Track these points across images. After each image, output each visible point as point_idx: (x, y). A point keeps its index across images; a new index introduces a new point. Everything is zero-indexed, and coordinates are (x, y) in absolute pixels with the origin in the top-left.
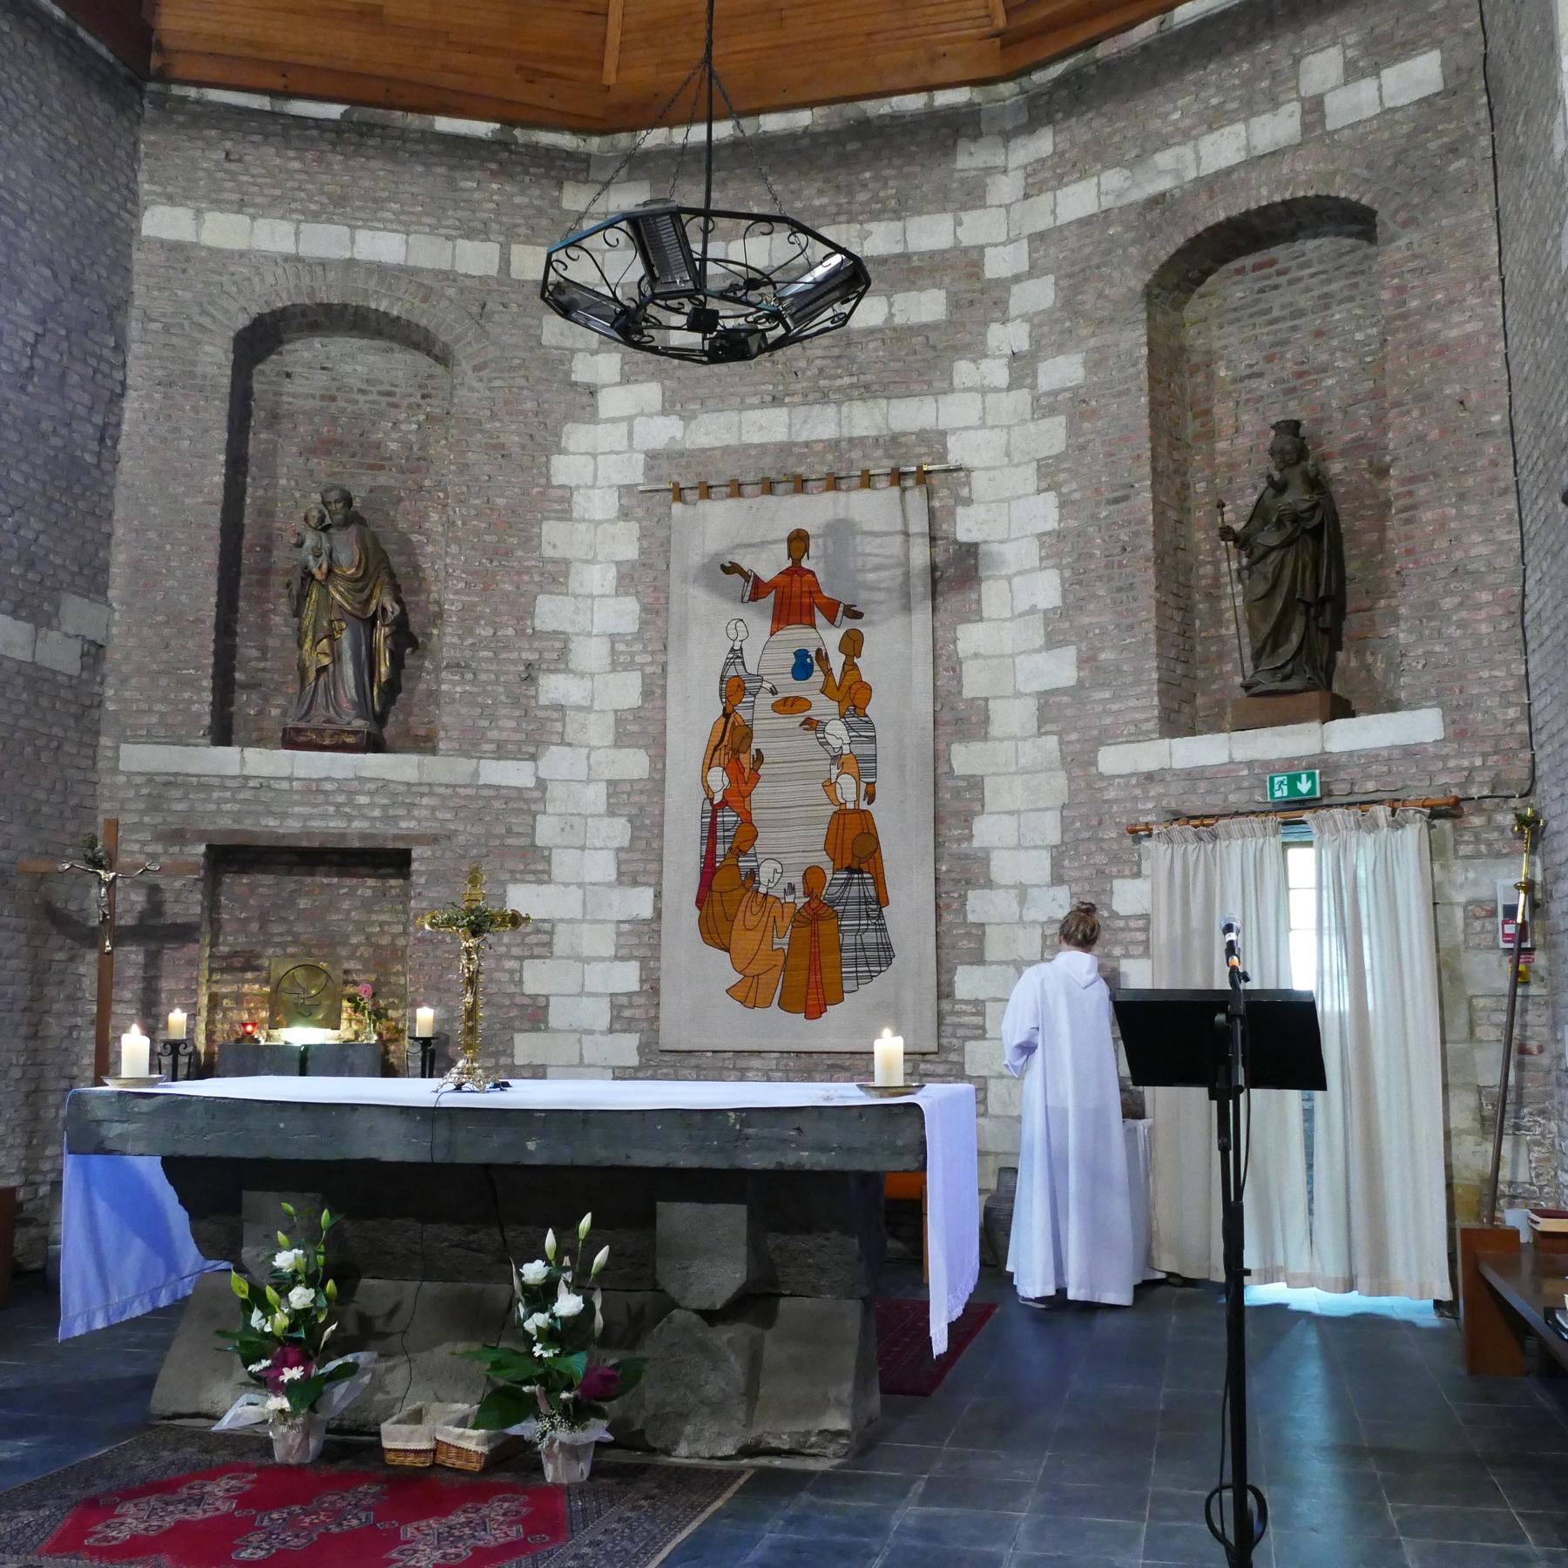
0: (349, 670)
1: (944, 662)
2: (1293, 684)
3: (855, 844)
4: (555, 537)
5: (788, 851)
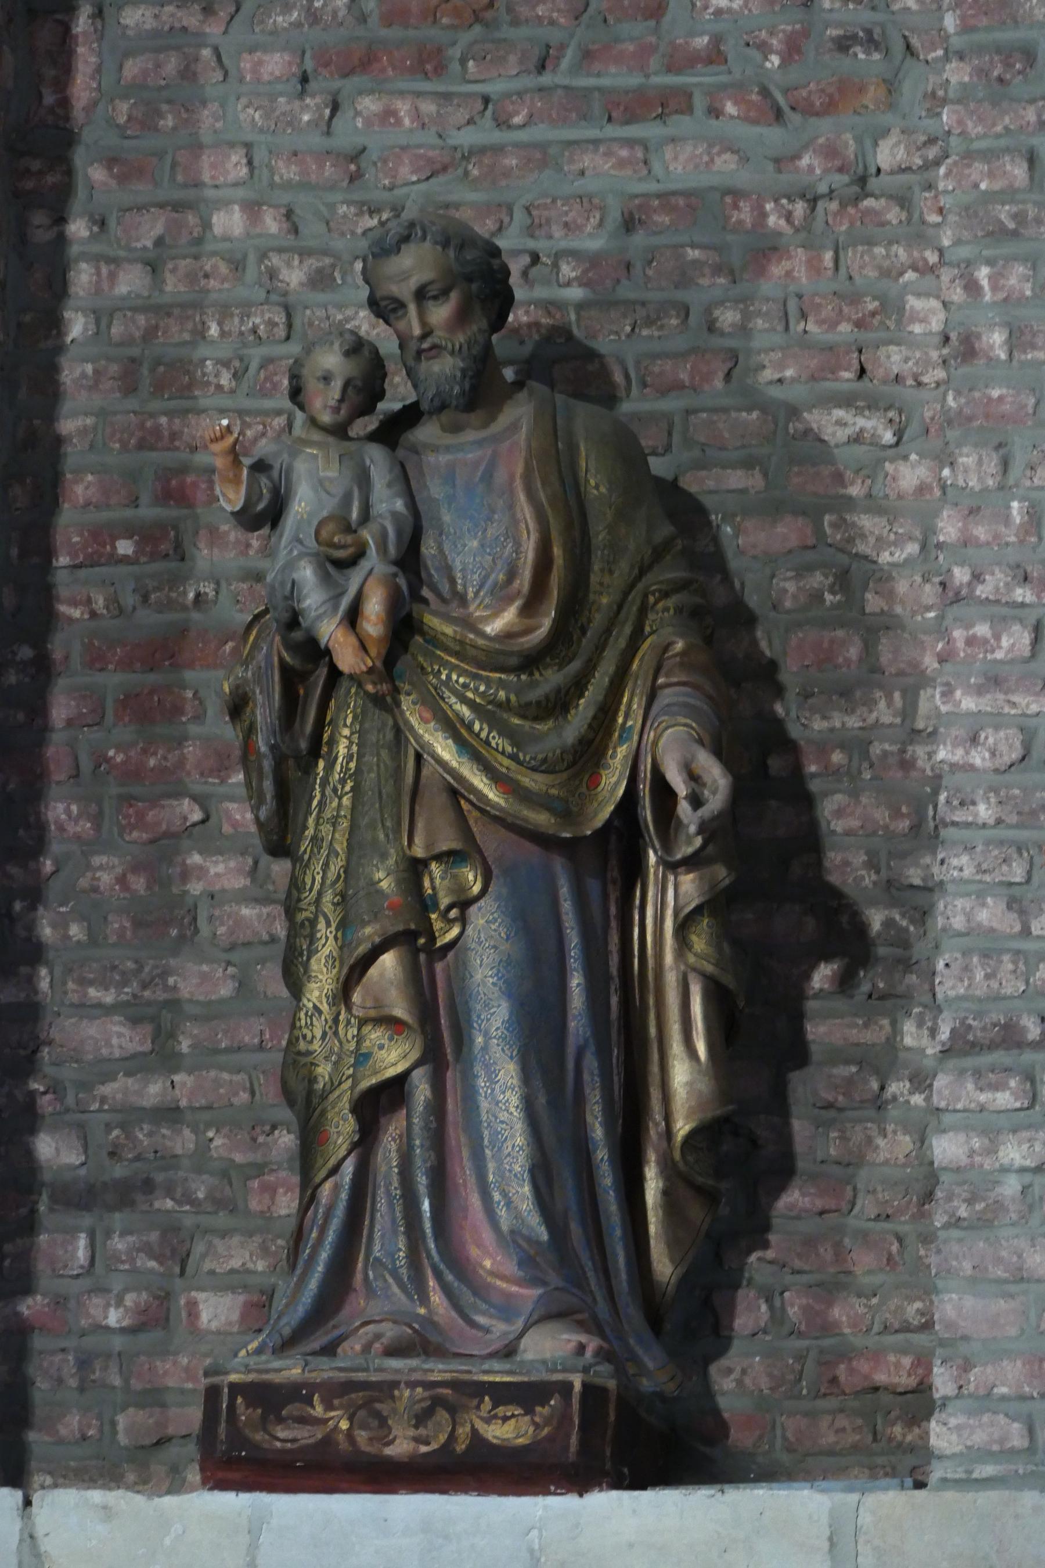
0: (500, 1092)
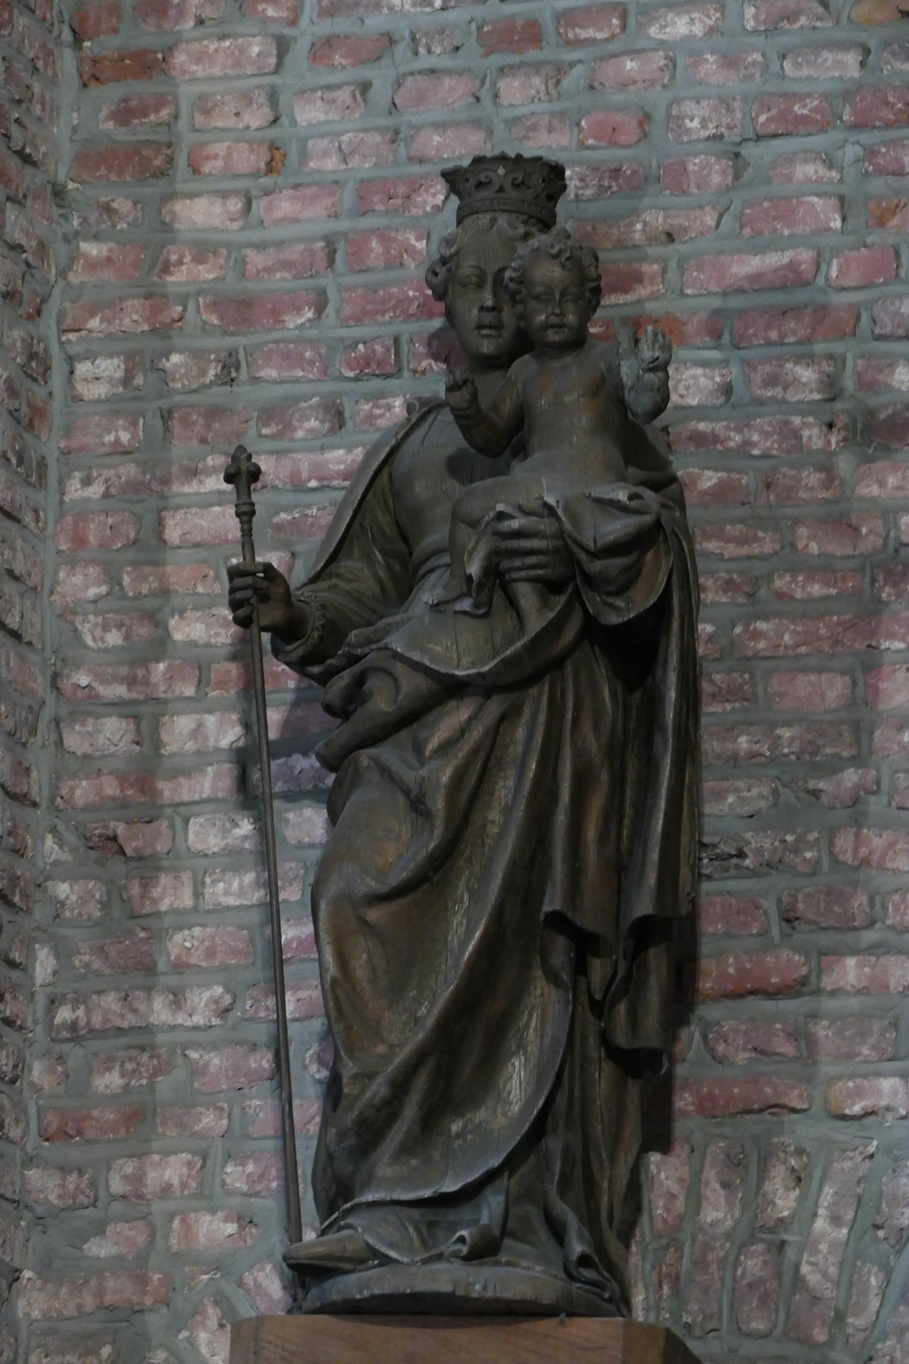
2: (522, 1275)
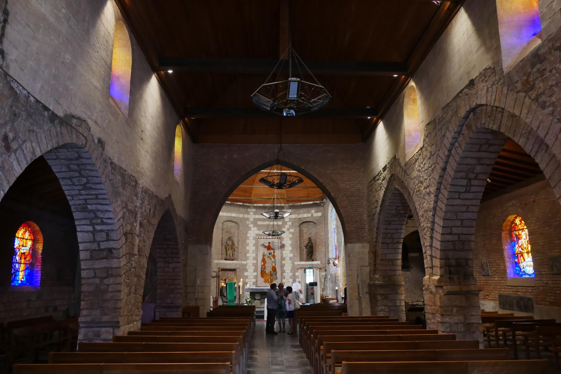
1: (282, 254)
3: (274, 269)
4: (248, 241)
5: (268, 270)
